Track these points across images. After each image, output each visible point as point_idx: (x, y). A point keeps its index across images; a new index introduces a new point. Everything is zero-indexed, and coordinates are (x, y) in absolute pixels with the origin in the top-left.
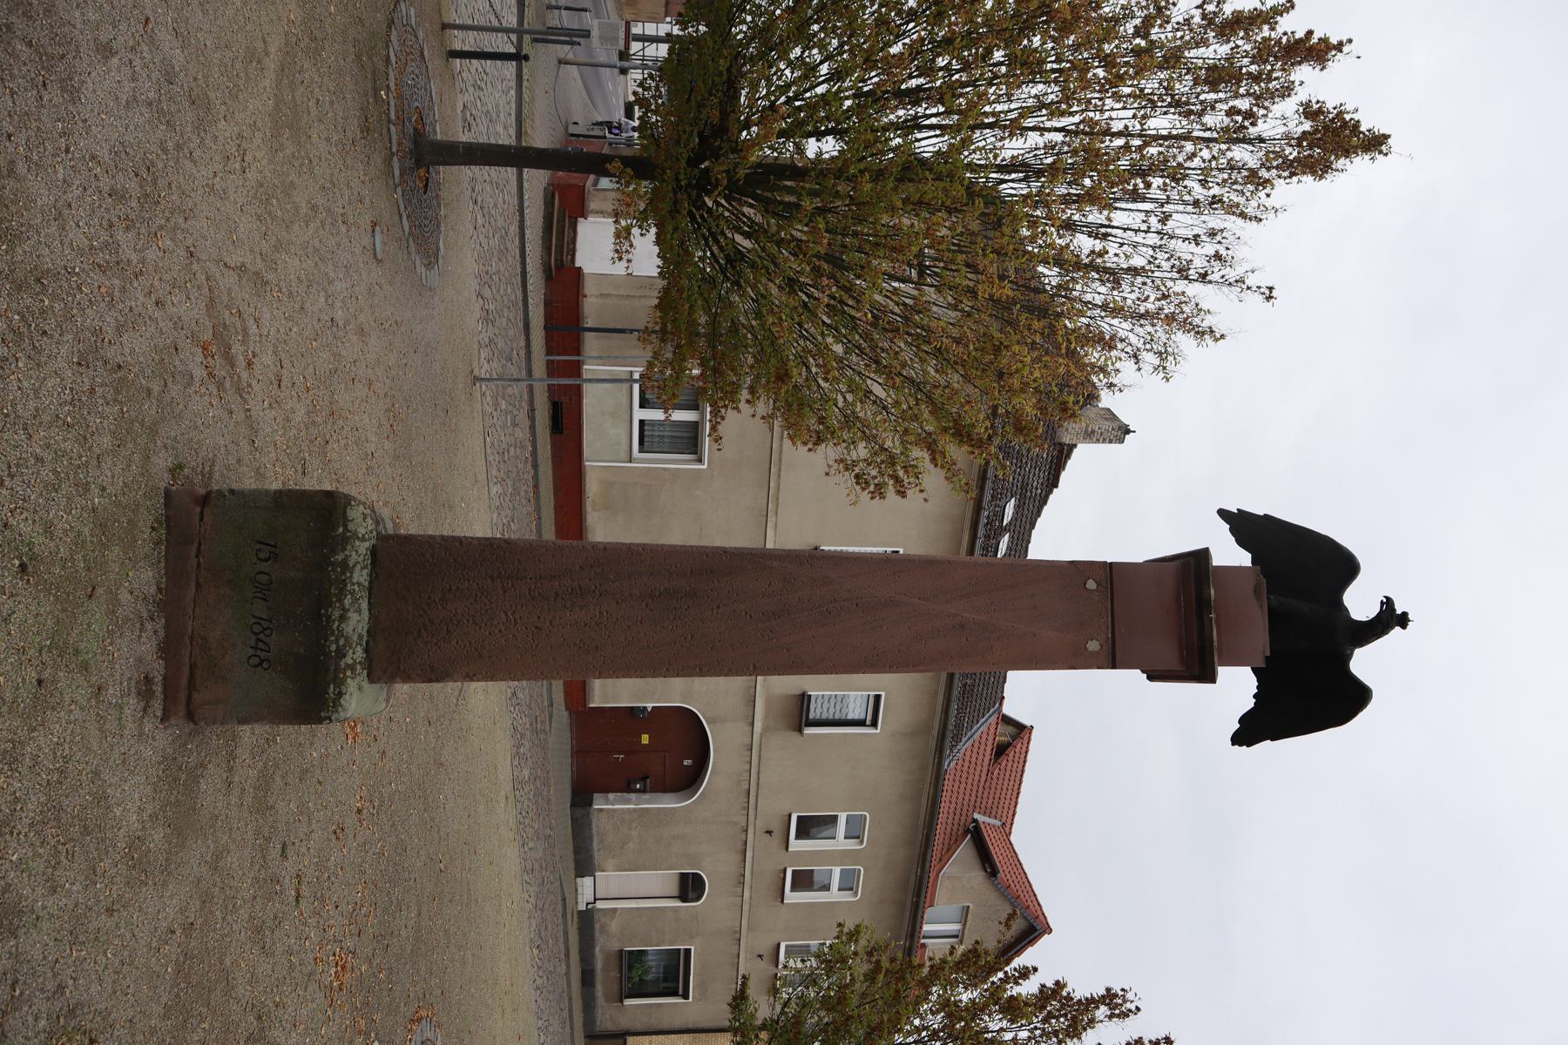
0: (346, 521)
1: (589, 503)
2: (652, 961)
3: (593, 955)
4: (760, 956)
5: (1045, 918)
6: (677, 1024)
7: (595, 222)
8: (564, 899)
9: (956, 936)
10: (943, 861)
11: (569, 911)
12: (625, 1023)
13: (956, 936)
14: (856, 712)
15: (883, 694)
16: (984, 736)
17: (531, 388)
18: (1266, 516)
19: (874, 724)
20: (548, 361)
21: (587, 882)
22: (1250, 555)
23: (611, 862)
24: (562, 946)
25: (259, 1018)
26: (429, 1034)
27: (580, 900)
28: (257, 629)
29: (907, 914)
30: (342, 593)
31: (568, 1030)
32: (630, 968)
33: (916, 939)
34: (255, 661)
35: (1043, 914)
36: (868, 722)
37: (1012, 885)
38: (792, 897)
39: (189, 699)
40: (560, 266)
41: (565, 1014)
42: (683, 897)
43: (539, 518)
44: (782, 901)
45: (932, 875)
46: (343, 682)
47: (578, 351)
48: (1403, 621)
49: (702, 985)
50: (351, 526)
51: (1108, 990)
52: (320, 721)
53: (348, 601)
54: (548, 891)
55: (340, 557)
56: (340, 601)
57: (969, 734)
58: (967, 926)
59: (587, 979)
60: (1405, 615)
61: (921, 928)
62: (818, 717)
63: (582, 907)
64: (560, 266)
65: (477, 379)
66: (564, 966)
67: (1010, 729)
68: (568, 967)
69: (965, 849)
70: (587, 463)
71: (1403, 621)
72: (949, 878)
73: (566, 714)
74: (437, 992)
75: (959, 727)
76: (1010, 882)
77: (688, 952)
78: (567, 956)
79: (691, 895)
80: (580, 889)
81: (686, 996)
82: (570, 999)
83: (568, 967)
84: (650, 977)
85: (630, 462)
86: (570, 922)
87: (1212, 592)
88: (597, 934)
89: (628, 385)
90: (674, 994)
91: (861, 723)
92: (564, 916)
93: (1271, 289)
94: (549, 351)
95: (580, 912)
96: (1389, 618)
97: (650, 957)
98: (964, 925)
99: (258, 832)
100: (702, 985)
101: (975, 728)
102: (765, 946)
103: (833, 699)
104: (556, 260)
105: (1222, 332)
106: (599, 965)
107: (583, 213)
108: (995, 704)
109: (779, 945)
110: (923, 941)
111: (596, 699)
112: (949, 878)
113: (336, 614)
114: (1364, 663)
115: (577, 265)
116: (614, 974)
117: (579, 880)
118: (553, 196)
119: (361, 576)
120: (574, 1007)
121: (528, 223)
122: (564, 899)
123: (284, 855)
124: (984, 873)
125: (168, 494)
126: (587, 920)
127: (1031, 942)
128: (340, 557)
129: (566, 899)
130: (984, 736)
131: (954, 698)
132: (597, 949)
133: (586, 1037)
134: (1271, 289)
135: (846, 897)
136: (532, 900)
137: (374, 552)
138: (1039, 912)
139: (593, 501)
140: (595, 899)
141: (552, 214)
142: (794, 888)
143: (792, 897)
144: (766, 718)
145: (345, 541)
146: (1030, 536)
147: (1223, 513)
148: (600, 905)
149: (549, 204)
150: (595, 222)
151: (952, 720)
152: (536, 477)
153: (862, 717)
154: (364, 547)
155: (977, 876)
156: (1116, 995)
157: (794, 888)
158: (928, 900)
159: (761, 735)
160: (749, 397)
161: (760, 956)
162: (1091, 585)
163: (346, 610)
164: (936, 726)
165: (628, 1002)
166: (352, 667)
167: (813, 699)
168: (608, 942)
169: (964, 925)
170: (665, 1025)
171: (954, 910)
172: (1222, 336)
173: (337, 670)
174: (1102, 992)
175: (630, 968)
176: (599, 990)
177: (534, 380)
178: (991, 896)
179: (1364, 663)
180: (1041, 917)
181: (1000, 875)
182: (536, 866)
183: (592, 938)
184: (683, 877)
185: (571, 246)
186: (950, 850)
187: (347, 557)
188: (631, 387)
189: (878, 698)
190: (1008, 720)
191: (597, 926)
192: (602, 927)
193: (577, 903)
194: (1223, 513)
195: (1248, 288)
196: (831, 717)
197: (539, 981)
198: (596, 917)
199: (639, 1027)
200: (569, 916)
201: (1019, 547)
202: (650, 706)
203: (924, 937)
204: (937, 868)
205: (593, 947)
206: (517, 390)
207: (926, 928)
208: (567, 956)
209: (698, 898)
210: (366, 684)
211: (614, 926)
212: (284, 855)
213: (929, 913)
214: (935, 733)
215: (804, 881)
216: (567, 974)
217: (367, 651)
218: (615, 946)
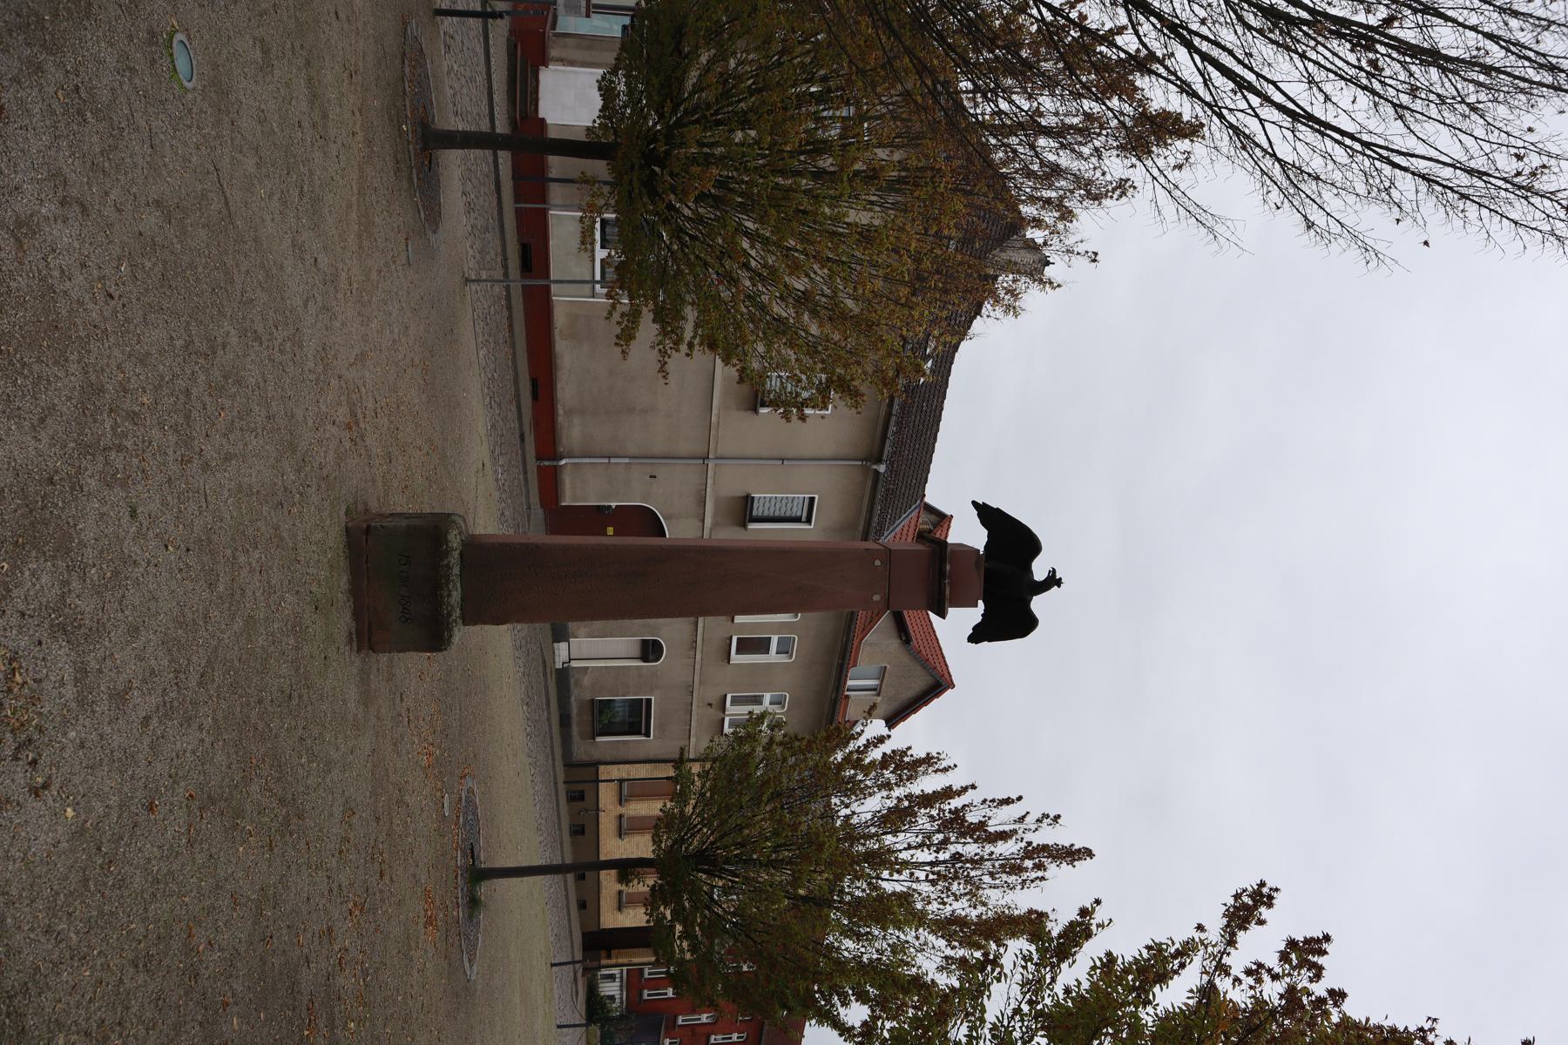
0: (447, 541)
1: (557, 332)
2: (619, 708)
3: (569, 703)
4: (710, 705)
5: (950, 676)
6: (641, 756)
7: (556, 70)
8: (544, 662)
9: (875, 690)
10: (865, 631)
11: (548, 671)
12: (596, 755)
13: (875, 690)
14: (796, 512)
15: (817, 496)
16: (905, 529)
17: (508, 289)
18: (998, 510)
19: (809, 521)
20: (516, 209)
21: (563, 646)
22: (986, 532)
23: (582, 631)
24: (544, 698)
25: (400, 791)
26: (470, 784)
27: (556, 660)
28: (403, 602)
29: (834, 672)
30: (447, 584)
31: (550, 762)
32: (601, 712)
33: (840, 692)
34: (403, 619)
35: (949, 673)
36: (803, 519)
37: (923, 651)
38: (736, 658)
39: (370, 638)
40: (525, 117)
41: (549, 749)
42: (645, 658)
43: (514, 353)
44: (729, 662)
45: (856, 643)
46: (451, 629)
47: (544, 201)
48: (1058, 583)
49: (661, 727)
50: (450, 544)
51: (928, 754)
52: (442, 650)
53: (451, 586)
54: (533, 659)
55: (445, 562)
56: (447, 586)
57: (891, 528)
58: (885, 682)
59: (565, 721)
60: (1060, 579)
61: (845, 683)
62: (760, 514)
63: (559, 666)
64: (525, 117)
65: (467, 281)
66: (546, 714)
67: (933, 518)
68: (549, 713)
69: (885, 621)
70: (554, 298)
71: (1058, 583)
72: (870, 645)
73: (540, 511)
74: (472, 756)
75: (881, 524)
76: (922, 648)
77: (649, 701)
78: (548, 705)
79: (651, 657)
80: (557, 653)
81: (648, 735)
82: (551, 738)
83: (549, 713)
84: (618, 719)
85: (593, 297)
86: (549, 678)
87: (948, 567)
88: (572, 686)
89: (590, 285)
90: (638, 733)
91: (797, 520)
92: (545, 674)
93: (1096, 254)
94: (517, 200)
95: (557, 670)
96: (1053, 581)
97: (617, 704)
98: (882, 681)
99: (390, 691)
100: (661, 727)
101: (898, 522)
102: (713, 696)
103: (773, 500)
104: (521, 112)
105: (1060, 282)
106: (574, 710)
107: (544, 61)
108: (916, 501)
109: (726, 696)
110: (847, 693)
111: (567, 498)
112: (870, 645)
113: (446, 594)
114: (1038, 604)
115: (541, 116)
116: (587, 717)
117: (556, 645)
118: (516, 46)
119: (456, 570)
120: (555, 744)
121: (495, 87)
122: (544, 662)
123: (402, 700)
124: (899, 641)
125: (347, 529)
126: (563, 677)
127: (938, 695)
128: (445, 562)
129: (546, 660)
130: (905, 529)
131: (877, 501)
132: (573, 699)
133: (564, 765)
134: (1096, 254)
135: (783, 659)
136: (522, 669)
137: (461, 554)
138: (945, 672)
139: (561, 331)
140: (570, 660)
141: (516, 66)
142: (738, 652)
143: (736, 658)
144: (715, 515)
145: (447, 553)
146: (953, 358)
147: (975, 504)
148: (574, 664)
149: (512, 54)
150: (556, 70)
151: (876, 519)
152: (510, 318)
153: (799, 514)
154: (456, 554)
155: (894, 644)
156: (933, 758)
157: (738, 652)
158: (851, 662)
159: (711, 530)
160: (688, 351)
161: (710, 705)
162: (878, 563)
163: (450, 591)
164: (862, 523)
165: (599, 739)
166: (455, 621)
167: (756, 502)
168: (580, 694)
169: (882, 681)
170: (631, 757)
171: (874, 669)
172: (1059, 286)
173: (448, 623)
174: (924, 756)
175: (601, 712)
176: (575, 730)
177: (511, 281)
178: (905, 659)
179: (1038, 604)
180: (946, 675)
181: (914, 642)
182: (523, 642)
183: (568, 690)
184: (645, 643)
185: (534, 96)
186: (872, 622)
187: (449, 562)
188: (594, 287)
189: (812, 500)
190: (930, 509)
191: (572, 681)
192: (576, 682)
193: (554, 662)
194: (975, 504)
195: (1078, 254)
196: (771, 514)
197: (529, 729)
198: (571, 673)
199: (609, 758)
200: (549, 675)
201: (943, 368)
202: (614, 504)
203: (848, 690)
204: (860, 636)
205: (569, 697)
206: (498, 289)
207: (850, 683)
208: (548, 705)
209: (657, 659)
210: (462, 627)
211: (586, 681)
212: (402, 700)
213: (852, 672)
214: (861, 529)
215: (746, 646)
216: (549, 719)
217: (461, 609)
218: (588, 696)
